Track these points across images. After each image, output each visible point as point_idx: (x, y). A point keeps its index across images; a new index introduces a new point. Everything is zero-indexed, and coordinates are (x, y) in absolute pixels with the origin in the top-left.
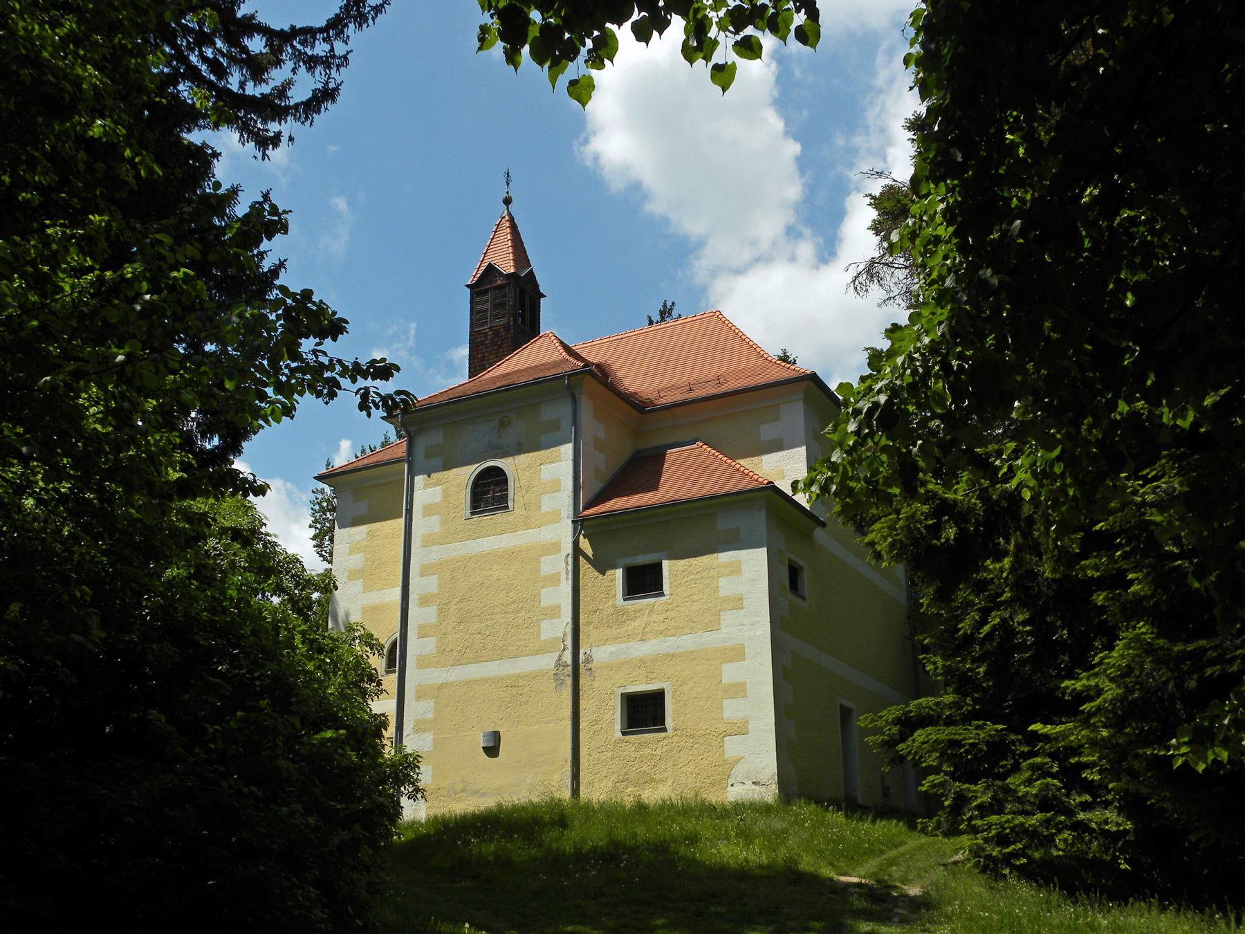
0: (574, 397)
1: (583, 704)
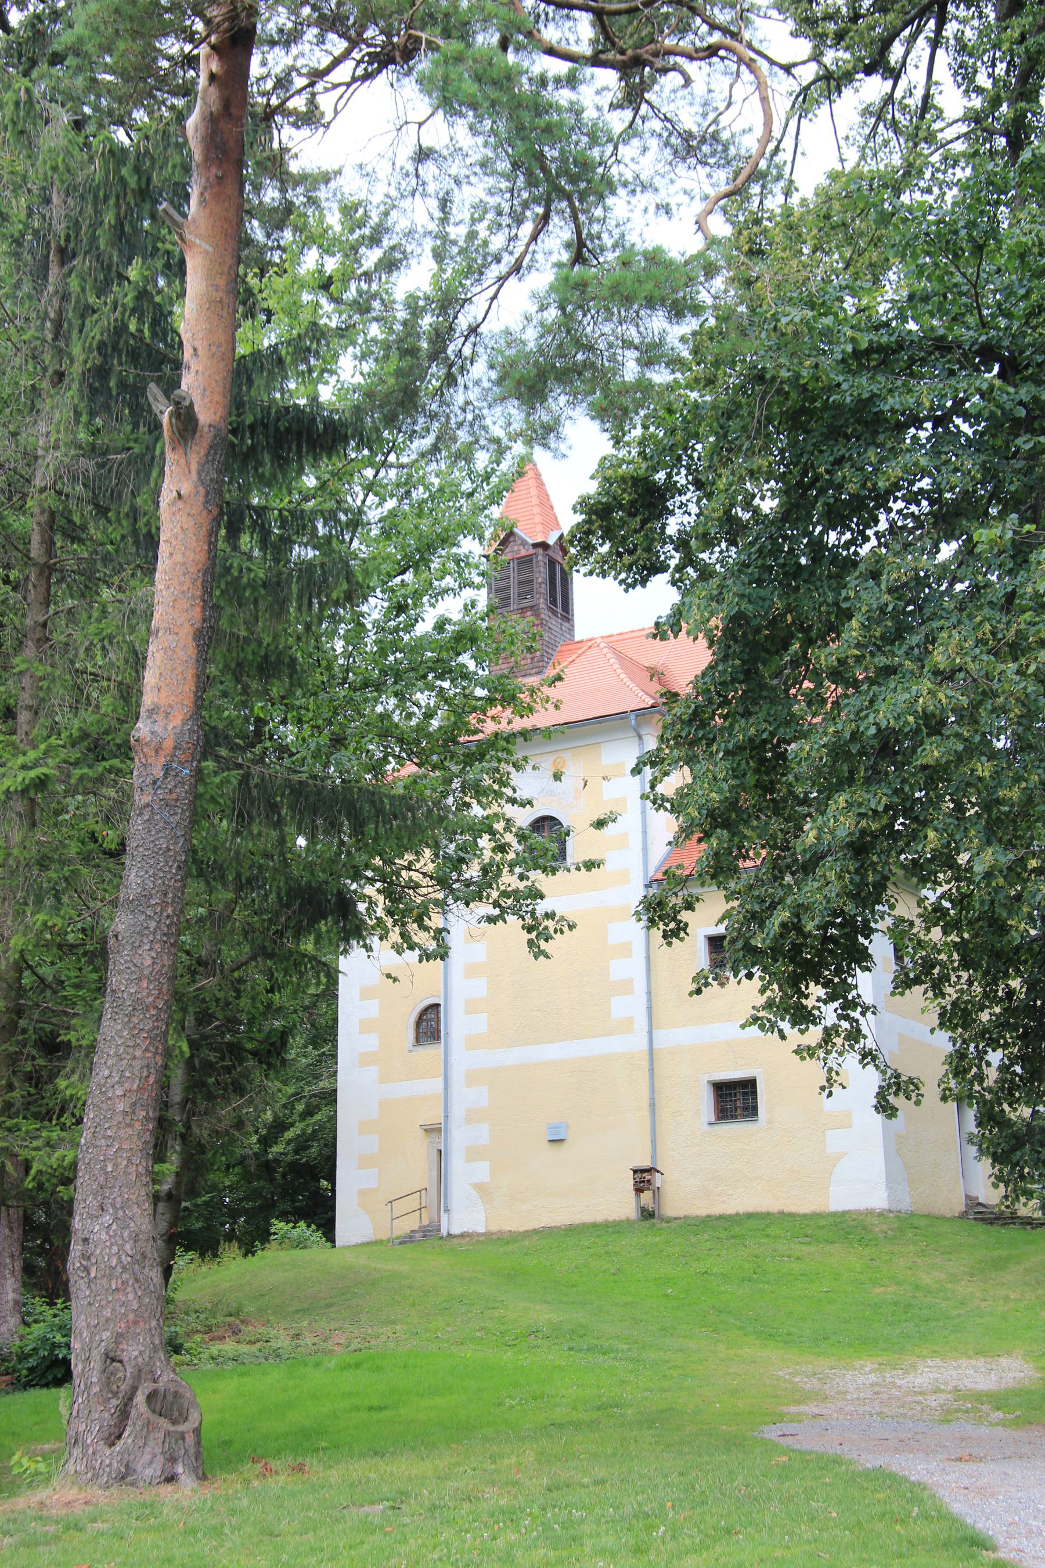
0: (640, 737)
1: (647, 1124)
